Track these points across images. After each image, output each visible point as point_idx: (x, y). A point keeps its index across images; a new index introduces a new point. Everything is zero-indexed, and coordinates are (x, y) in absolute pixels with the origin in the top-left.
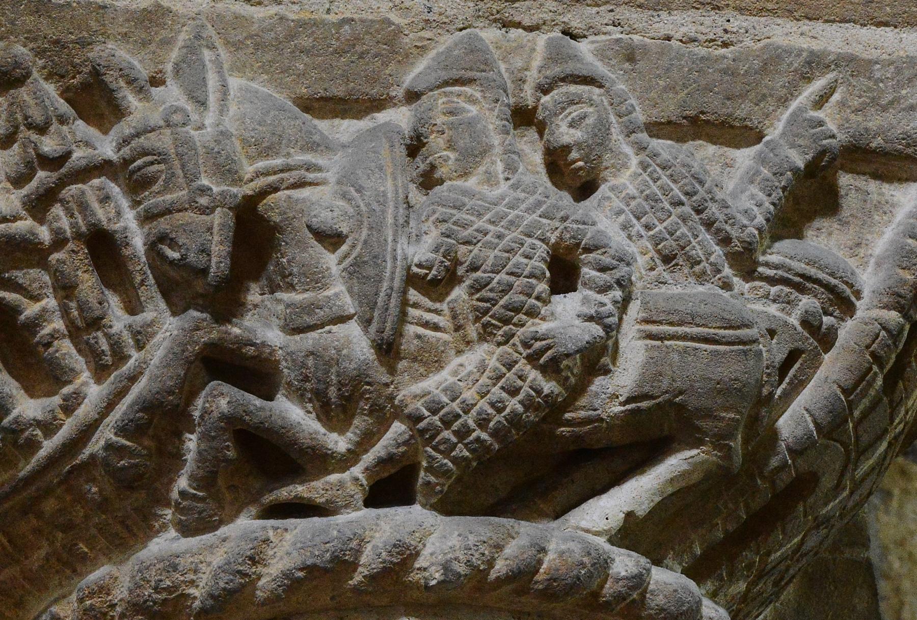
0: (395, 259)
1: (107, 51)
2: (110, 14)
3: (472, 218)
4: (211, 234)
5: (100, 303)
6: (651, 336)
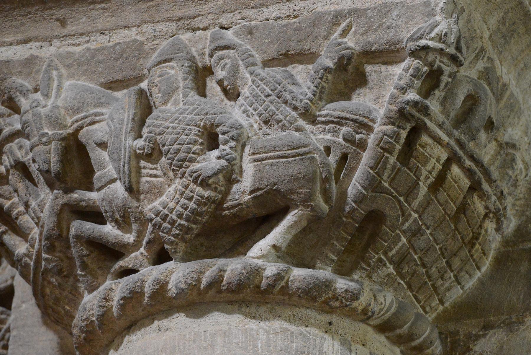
0: (125, 148)
3: (163, 122)
6: (255, 161)
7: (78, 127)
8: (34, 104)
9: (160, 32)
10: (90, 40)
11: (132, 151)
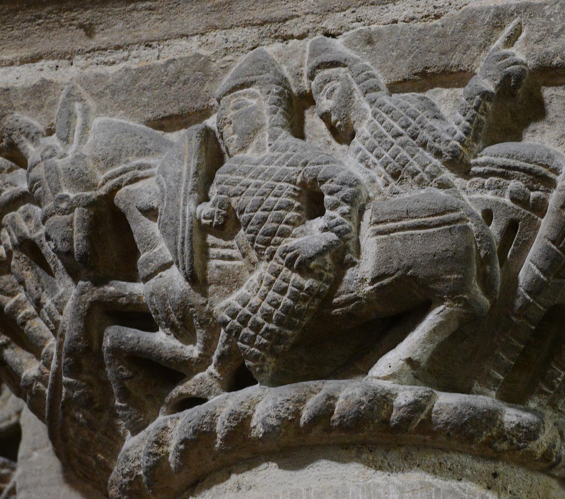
0: (184, 217)
2: (12, 94)
4: (72, 226)
6: (380, 233)
7: (114, 185)
8: (48, 153)
9: (234, 42)
10: (129, 56)
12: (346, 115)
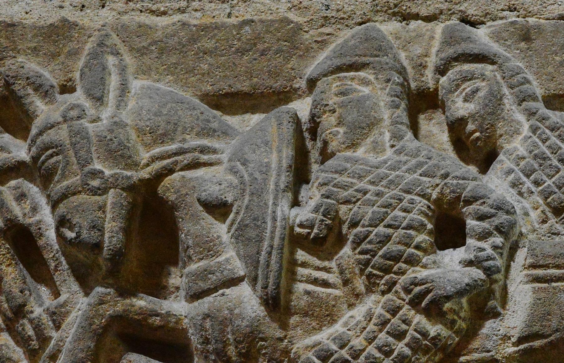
0: (274, 219)
1: (17, 64)
3: (354, 181)
4: (104, 212)
5: (21, 292)
6: (537, 279)
7: (164, 168)
8: (74, 113)
9: (338, 11)
10: (188, 7)
11: (287, 228)
12: (492, 126)
